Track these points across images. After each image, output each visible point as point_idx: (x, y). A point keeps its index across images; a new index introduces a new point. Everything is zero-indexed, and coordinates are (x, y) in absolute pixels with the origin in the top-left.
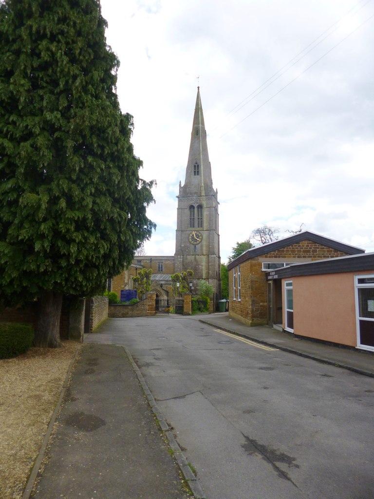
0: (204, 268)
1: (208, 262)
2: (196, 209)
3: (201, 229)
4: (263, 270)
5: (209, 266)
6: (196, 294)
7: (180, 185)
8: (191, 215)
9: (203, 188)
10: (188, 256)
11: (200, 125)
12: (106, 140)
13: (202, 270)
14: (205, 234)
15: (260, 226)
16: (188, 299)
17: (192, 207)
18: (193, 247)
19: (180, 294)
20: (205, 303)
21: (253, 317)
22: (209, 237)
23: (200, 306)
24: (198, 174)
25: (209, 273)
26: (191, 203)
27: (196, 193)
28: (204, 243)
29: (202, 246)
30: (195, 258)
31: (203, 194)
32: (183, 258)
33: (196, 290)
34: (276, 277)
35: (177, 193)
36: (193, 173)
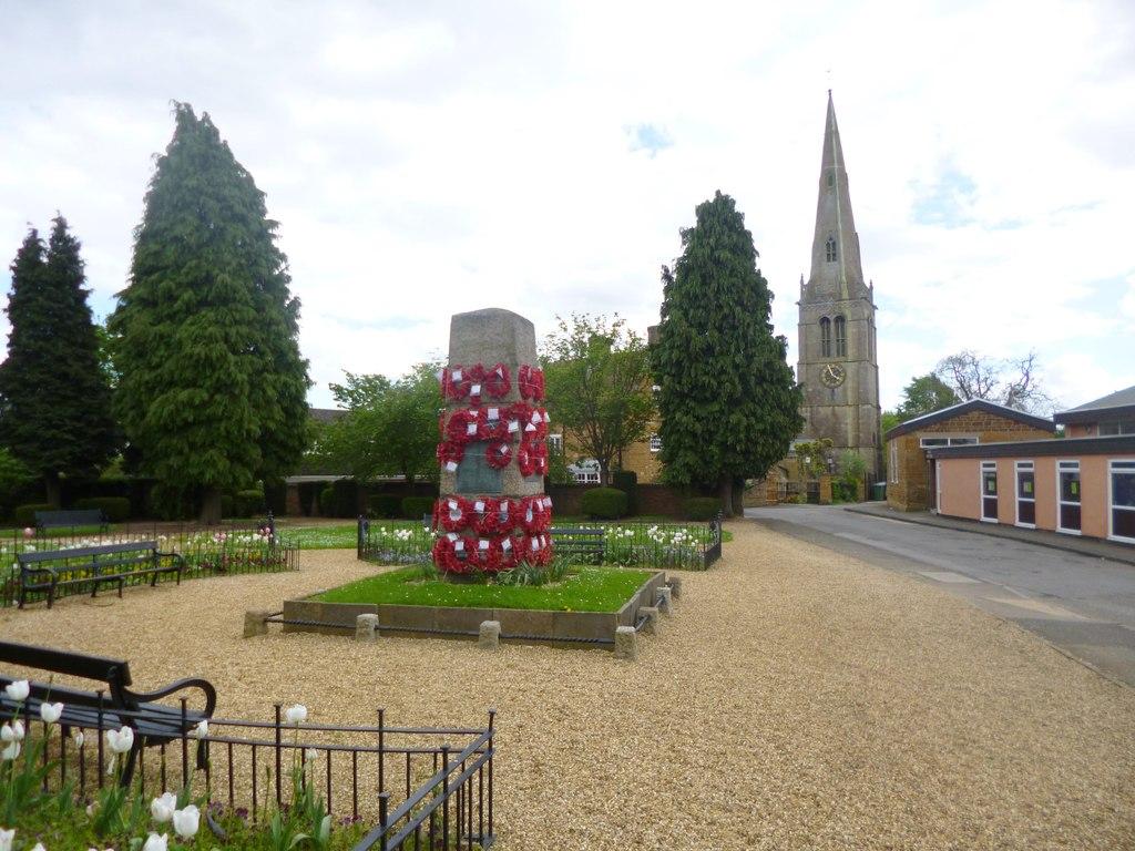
0: (849, 427)
1: (857, 417)
2: (832, 324)
3: (842, 358)
4: (921, 446)
5: (858, 424)
6: (837, 474)
7: (802, 281)
8: (823, 335)
9: (844, 286)
10: (820, 409)
11: (836, 166)
12: (774, 370)
13: (846, 432)
14: (850, 369)
15: (956, 352)
16: (826, 485)
17: (824, 321)
18: (828, 391)
19: (812, 475)
20: (853, 488)
21: (909, 501)
22: (858, 372)
23: (845, 493)
24: (834, 260)
25: (859, 437)
26: (823, 313)
27: (831, 295)
28: (850, 384)
29: (845, 390)
30: (833, 410)
31: (845, 295)
32: (811, 412)
33: (837, 466)
34: (931, 456)
35: (798, 297)
36: (825, 258)
